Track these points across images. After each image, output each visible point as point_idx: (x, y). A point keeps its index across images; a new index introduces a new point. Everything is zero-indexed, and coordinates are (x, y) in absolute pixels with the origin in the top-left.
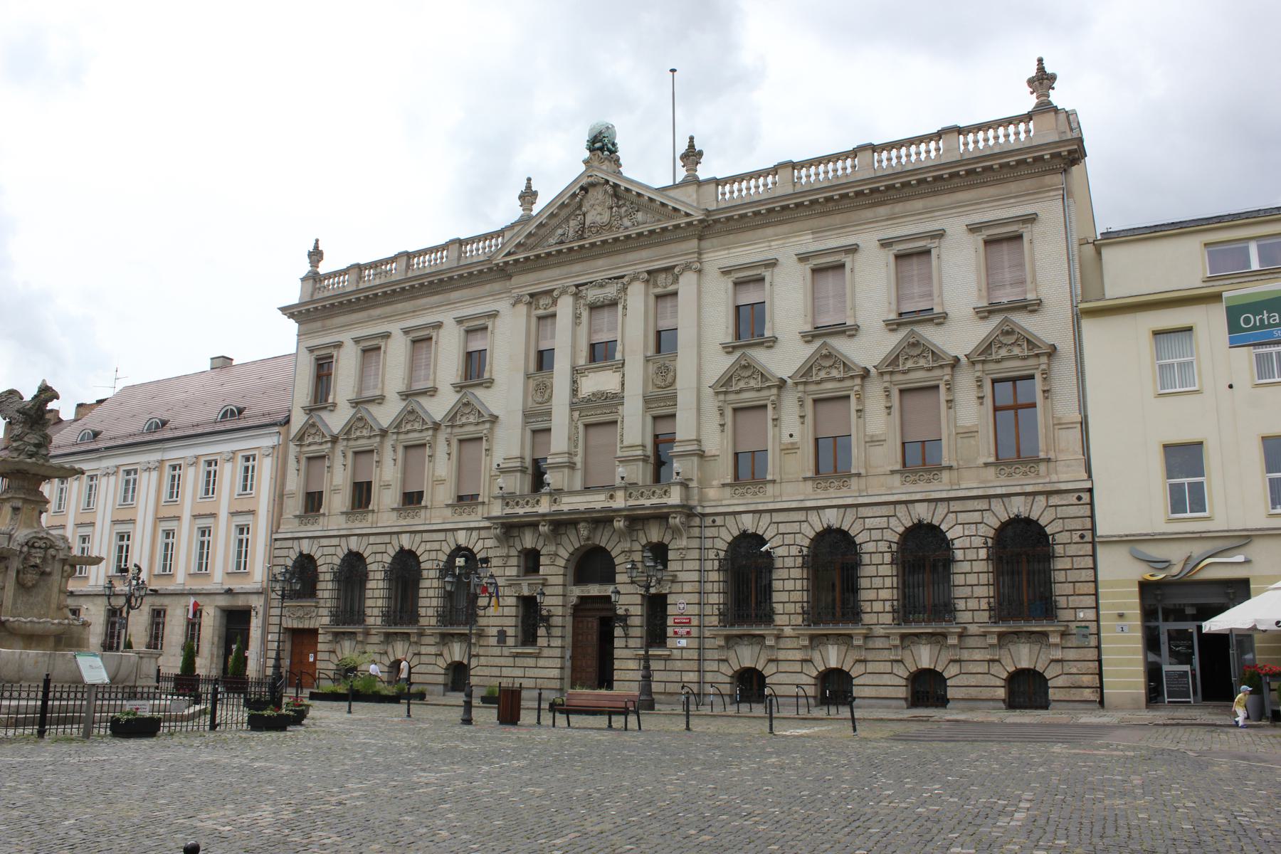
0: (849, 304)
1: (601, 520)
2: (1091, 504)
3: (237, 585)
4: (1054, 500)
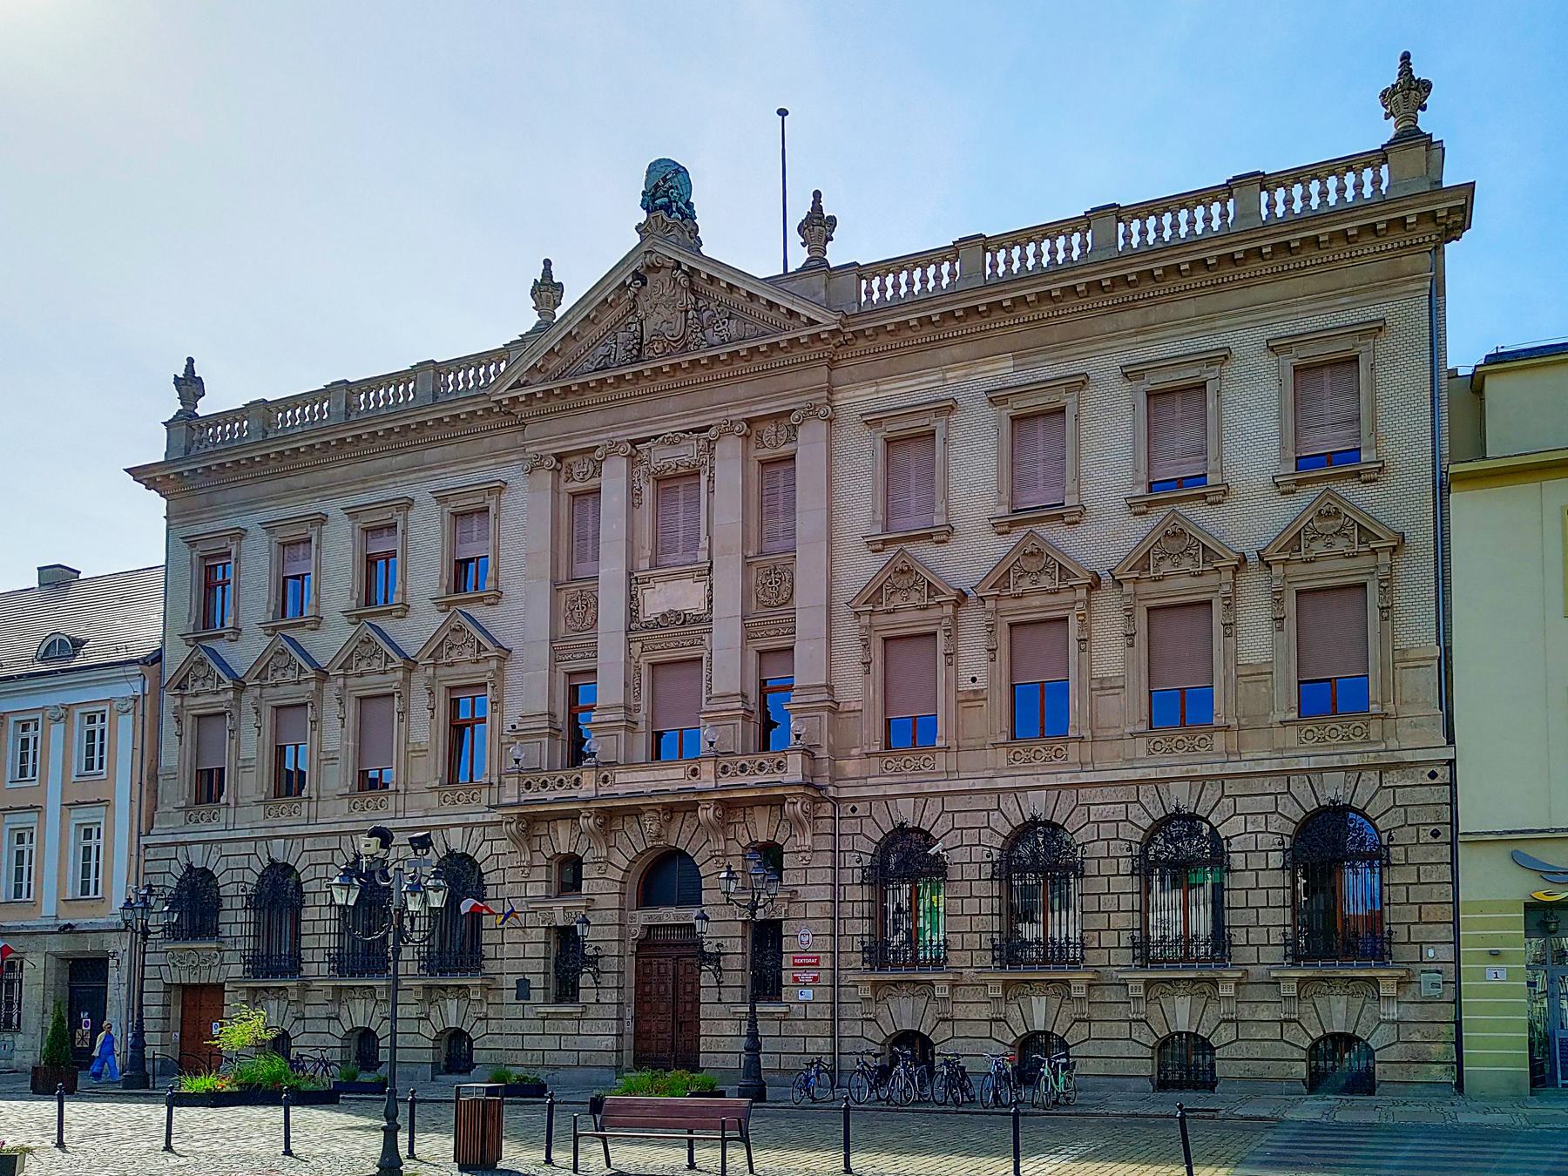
0: (1069, 475)
1: (678, 808)
2: (1453, 783)
3: (80, 917)
4: (1392, 778)
